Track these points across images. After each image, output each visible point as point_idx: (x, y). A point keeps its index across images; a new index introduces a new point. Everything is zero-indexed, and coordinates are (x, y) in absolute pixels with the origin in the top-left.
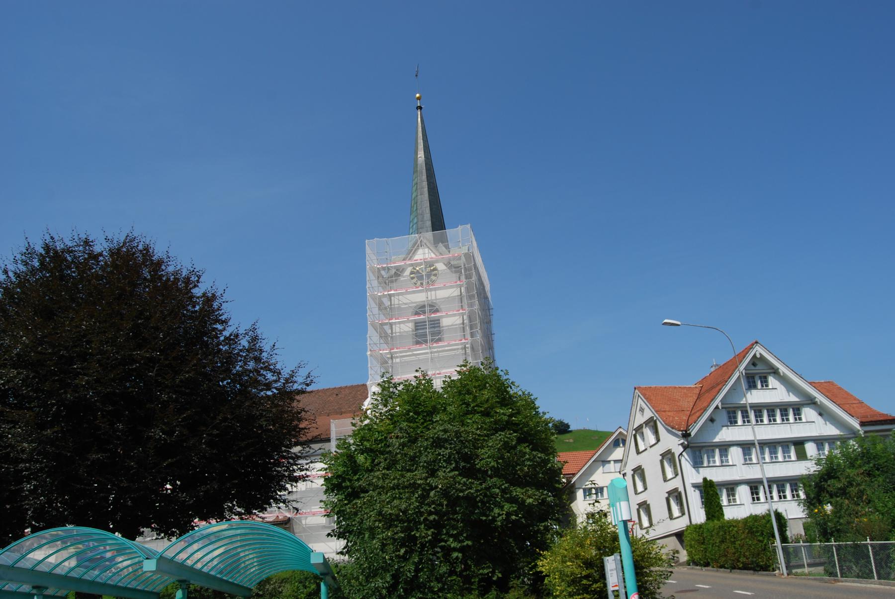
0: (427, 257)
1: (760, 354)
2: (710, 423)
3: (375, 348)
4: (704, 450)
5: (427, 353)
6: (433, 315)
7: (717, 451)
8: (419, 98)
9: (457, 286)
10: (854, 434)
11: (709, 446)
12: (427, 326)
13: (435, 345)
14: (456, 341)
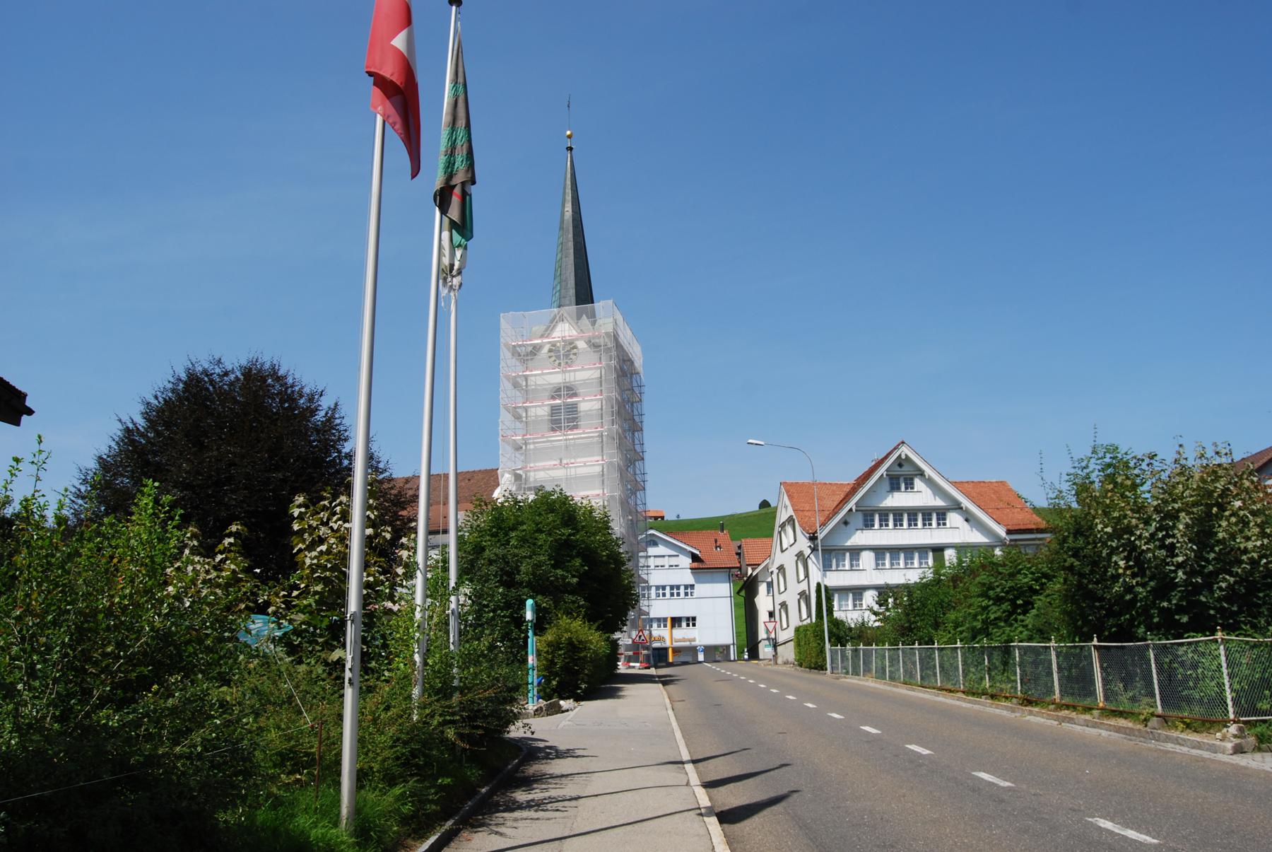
0: (567, 334)
1: (906, 455)
2: (843, 526)
3: (509, 433)
4: (833, 553)
5: (561, 440)
6: (569, 400)
7: (848, 555)
8: (569, 137)
11: (839, 550)
13: (569, 432)
14: (591, 428)
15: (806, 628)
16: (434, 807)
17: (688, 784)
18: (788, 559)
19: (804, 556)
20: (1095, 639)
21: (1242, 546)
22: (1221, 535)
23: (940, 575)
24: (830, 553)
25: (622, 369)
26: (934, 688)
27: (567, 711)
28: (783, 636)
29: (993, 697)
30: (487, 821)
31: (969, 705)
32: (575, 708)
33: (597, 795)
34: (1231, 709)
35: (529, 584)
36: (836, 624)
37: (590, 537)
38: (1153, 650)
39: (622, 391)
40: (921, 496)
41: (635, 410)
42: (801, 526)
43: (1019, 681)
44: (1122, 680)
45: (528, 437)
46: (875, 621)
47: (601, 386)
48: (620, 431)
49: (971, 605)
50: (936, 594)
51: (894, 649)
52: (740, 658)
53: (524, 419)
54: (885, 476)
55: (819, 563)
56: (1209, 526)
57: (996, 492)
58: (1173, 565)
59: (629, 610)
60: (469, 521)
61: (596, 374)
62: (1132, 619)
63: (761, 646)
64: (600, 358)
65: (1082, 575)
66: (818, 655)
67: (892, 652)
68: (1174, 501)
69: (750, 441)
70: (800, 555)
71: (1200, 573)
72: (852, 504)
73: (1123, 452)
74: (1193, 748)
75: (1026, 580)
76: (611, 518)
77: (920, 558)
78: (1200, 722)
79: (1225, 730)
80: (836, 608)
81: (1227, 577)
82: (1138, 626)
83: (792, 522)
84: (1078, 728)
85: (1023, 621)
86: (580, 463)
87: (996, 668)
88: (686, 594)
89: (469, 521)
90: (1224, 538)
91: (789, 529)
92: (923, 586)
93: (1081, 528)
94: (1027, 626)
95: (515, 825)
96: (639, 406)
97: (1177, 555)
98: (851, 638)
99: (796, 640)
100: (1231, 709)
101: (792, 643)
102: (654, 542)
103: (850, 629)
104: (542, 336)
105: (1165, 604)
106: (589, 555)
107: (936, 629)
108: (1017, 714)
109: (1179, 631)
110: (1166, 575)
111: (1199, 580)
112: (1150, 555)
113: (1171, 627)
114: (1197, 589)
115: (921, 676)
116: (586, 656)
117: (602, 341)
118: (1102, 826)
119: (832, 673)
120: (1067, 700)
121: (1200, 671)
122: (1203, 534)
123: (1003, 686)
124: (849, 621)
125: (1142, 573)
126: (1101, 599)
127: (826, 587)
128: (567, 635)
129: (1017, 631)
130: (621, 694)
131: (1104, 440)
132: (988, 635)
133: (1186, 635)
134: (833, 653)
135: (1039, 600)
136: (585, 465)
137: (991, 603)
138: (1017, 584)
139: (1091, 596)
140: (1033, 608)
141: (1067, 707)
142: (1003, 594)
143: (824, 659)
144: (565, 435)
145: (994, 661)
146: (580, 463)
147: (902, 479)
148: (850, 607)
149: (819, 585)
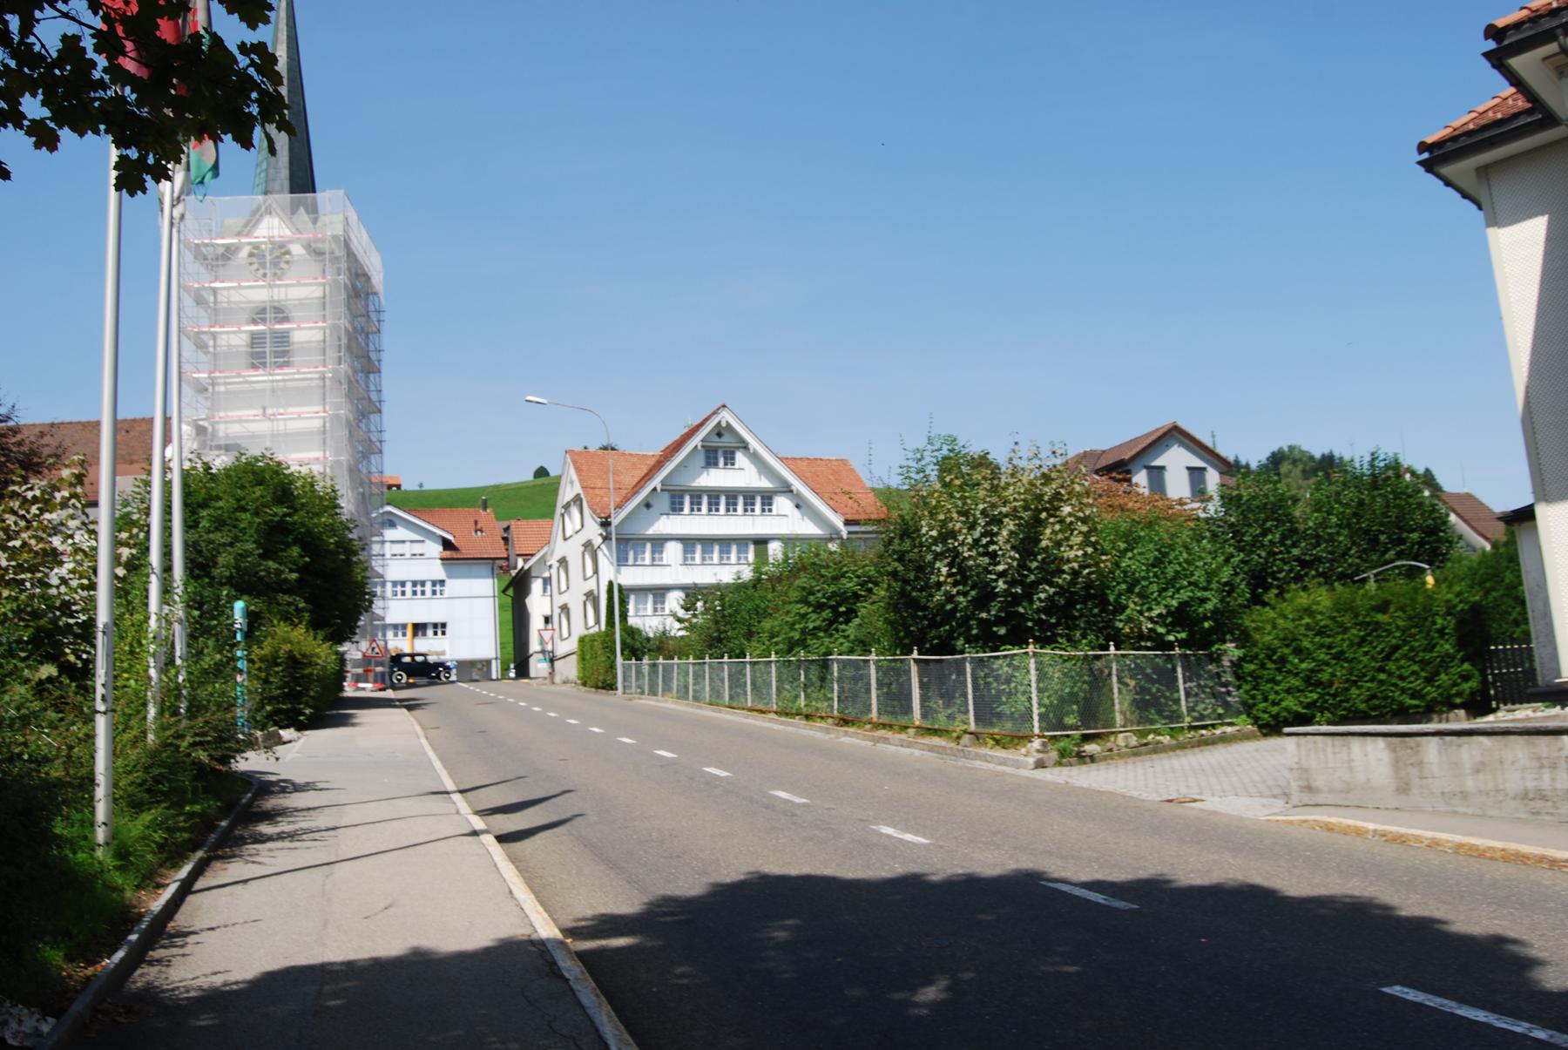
0: (276, 233)
2: (645, 509)
4: (631, 543)
6: (278, 326)
7: (649, 546)
9: (318, 284)
10: (834, 536)
12: (268, 340)
13: (278, 371)
14: (309, 367)
15: (593, 638)
16: (186, 835)
17: (458, 812)
18: (571, 549)
19: (593, 546)
20: (915, 652)
21: (1066, 555)
22: (1044, 543)
23: (761, 574)
24: (626, 544)
25: (353, 286)
26: (743, 709)
27: (290, 742)
28: (562, 648)
29: (808, 717)
30: (237, 853)
31: (781, 727)
32: (299, 738)
33: (245, 881)
34: (1036, 724)
35: (230, 582)
36: (631, 633)
37: (312, 518)
38: (970, 663)
39: (354, 316)
40: (742, 475)
41: (371, 345)
42: (591, 507)
43: (836, 699)
44: (942, 696)
45: (217, 374)
46: (679, 629)
47: (324, 309)
48: (350, 372)
49: (788, 612)
50: (751, 599)
51: (699, 664)
52: (504, 676)
53: (211, 350)
54: (699, 447)
55: (611, 555)
56: (1035, 532)
57: (834, 472)
58: (995, 574)
59: (361, 614)
60: (140, 494)
61: (318, 292)
62: (952, 631)
63: (532, 661)
64: (324, 271)
65: (906, 582)
66: (607, 672)
67: (697, 667)
68: (1005, 504)
69: (529, 398)
70: (588, 545)
71: (1021, 583)
72: (656, 482)
73: (961, 444)
74: (1000, 764)
75: (851, 585)
76: (339, 493)
77: (739, 552)
78: (1009, 738)
79: (1029, 745)
80: (631, 612)
81: (1047, 588)
82: (957, 638)
83: (578, 503)
84: (892, 748)
85: (844, 631)
86: (292, 414)
87: (812, 684)
88: (434, 593)
89: (140, 494)
90: (1047, 546)
91: (575, 511)
92: (739, 587)
93: (908, 531)
94: (848, 636)
95: (272, 854)
96: (377, 339)
97: (999, 563)
98: (649, 650)
99: (579, 653)
100: (1036, 724)
101: (574, 657)
102: (391, 523)
103: (648, 639)
104: (239, 234)
105: (984, 615)
106: (310, 543)
107: (749, 640)
108: (832, 736)
109: (994, 643)
110: (988, 584)
111: (1019, 591)
112: (971, 563)
113: (989, 640)
114: (1017, 600)
115: (730, 695)
116: (311, 674)
117: (326, 247)
118: (884, 831)
119: (624, 693)
120: (885, 719)
121: (1013, 685)
122: (1027, 544)
123: (819, 705)
124: (647, 629)
125: (964, 582)
126: (925, 608)
127: (620, 586)
128: (287, 647)
129: (838, 642)
130: (355, 721)
131: (942, 429)
132: (805, 647)
133: (1002, 648)
134: (626, 669)
135: (864, 607)
136: (299, 418)
137: (811, 609)
138: (840, 589)
139: (914, 605)
140: (857, 617)
141: (884, 726)
142: (824, 600)
143: (615, 676)
144: (271, 375)
145: (811, 676)
146: (292, 414)
147: (720, 453)
148: (650, 611)
149: (611, 584)
